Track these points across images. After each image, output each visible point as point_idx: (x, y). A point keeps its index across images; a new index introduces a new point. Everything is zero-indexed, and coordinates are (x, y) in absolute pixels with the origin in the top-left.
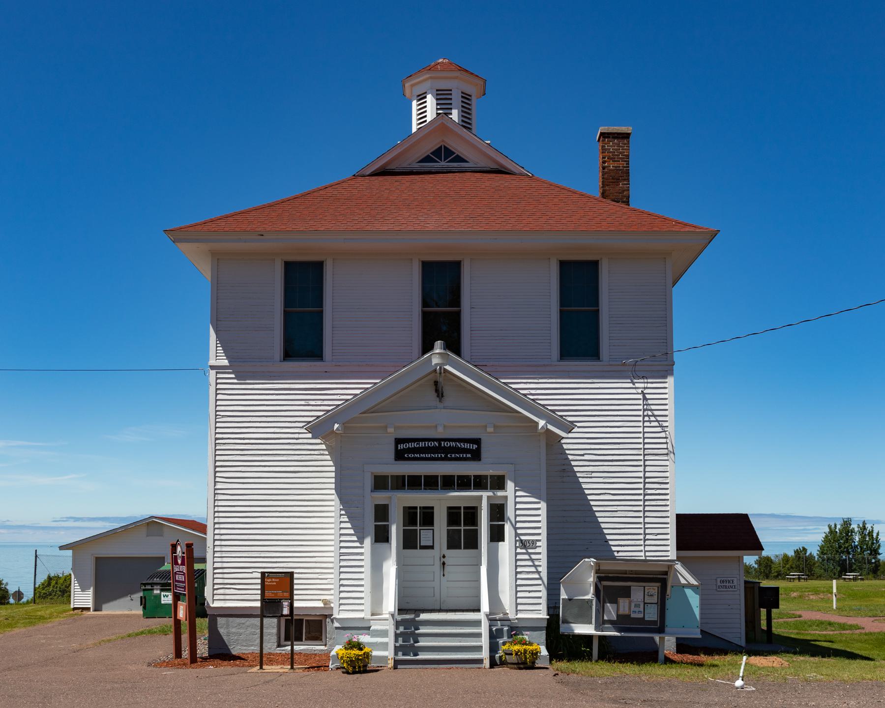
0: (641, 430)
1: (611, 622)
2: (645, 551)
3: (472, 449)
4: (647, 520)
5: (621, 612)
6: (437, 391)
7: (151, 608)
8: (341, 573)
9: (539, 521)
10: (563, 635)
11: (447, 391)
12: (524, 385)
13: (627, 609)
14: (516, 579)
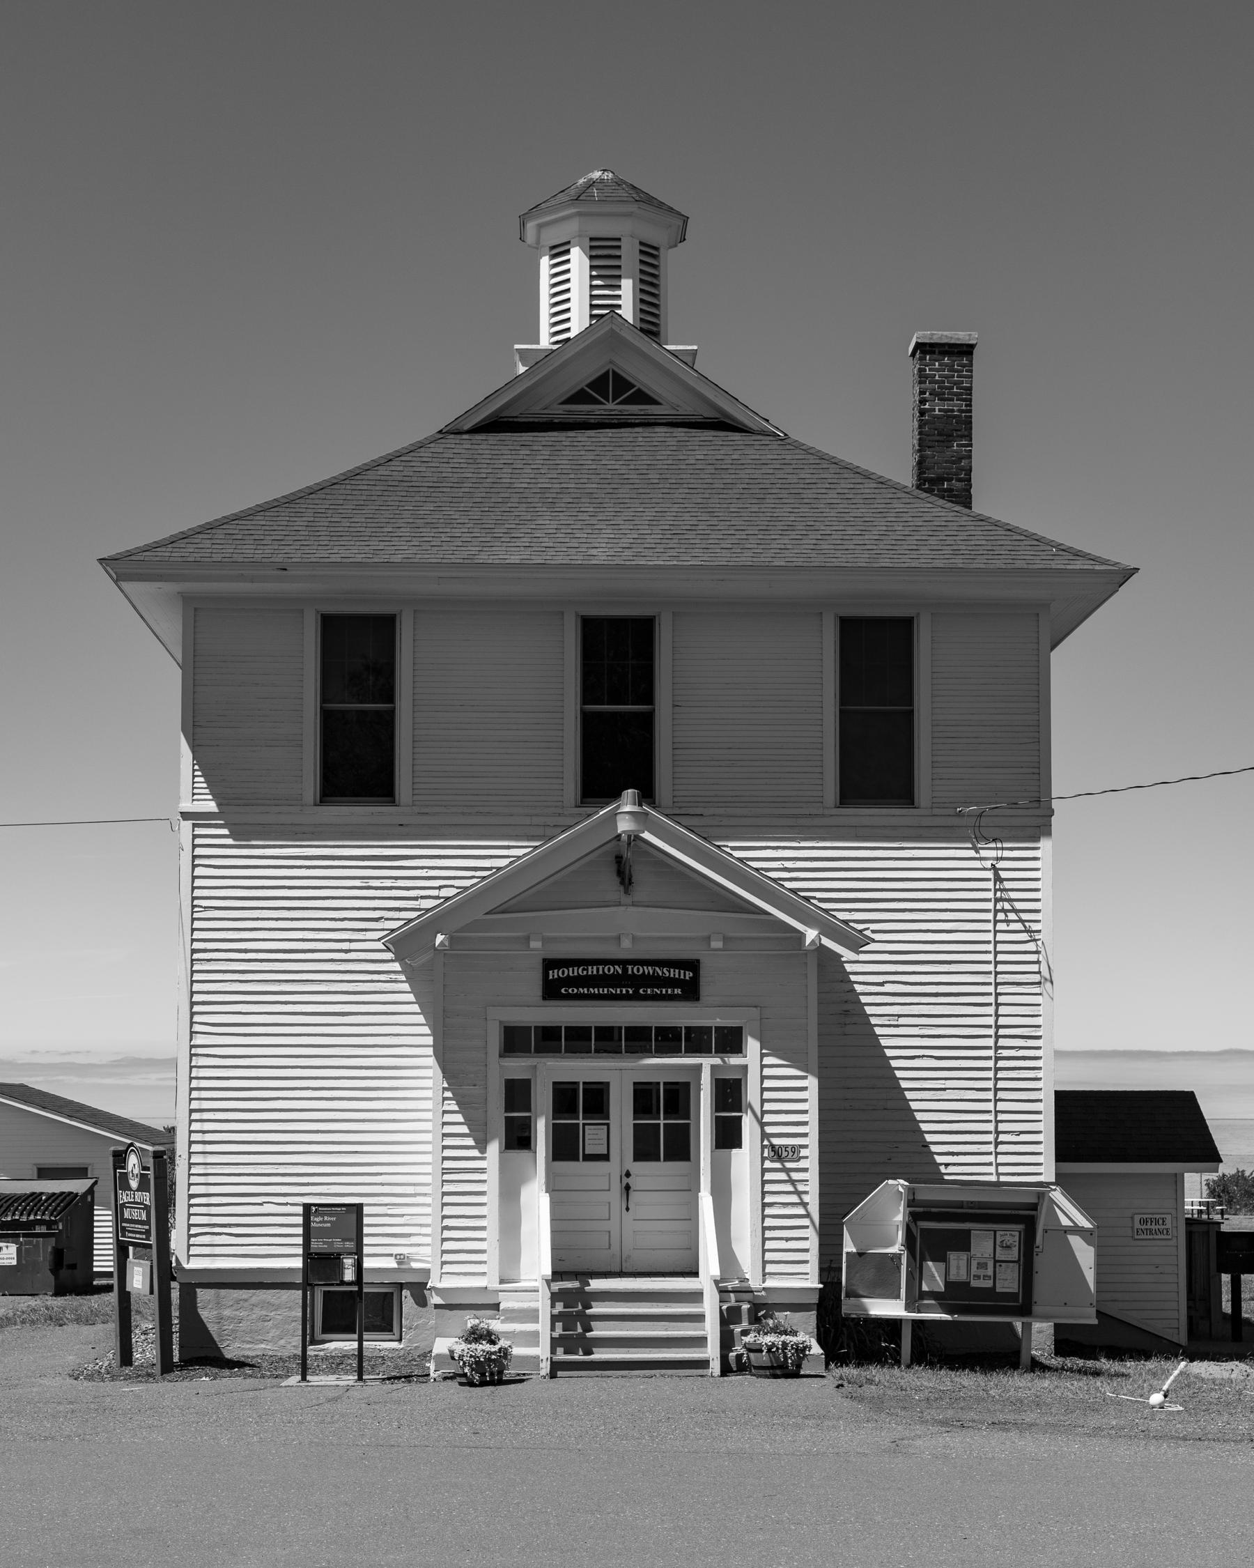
0: (990, 937)
2: (998, 1165)
3: (684, 979)
4: (1001, 1106)
8: (444, 1205)
9: (806, 1112)
10: (848, 1318)
11: (640, 873)
13: (963, 1272)
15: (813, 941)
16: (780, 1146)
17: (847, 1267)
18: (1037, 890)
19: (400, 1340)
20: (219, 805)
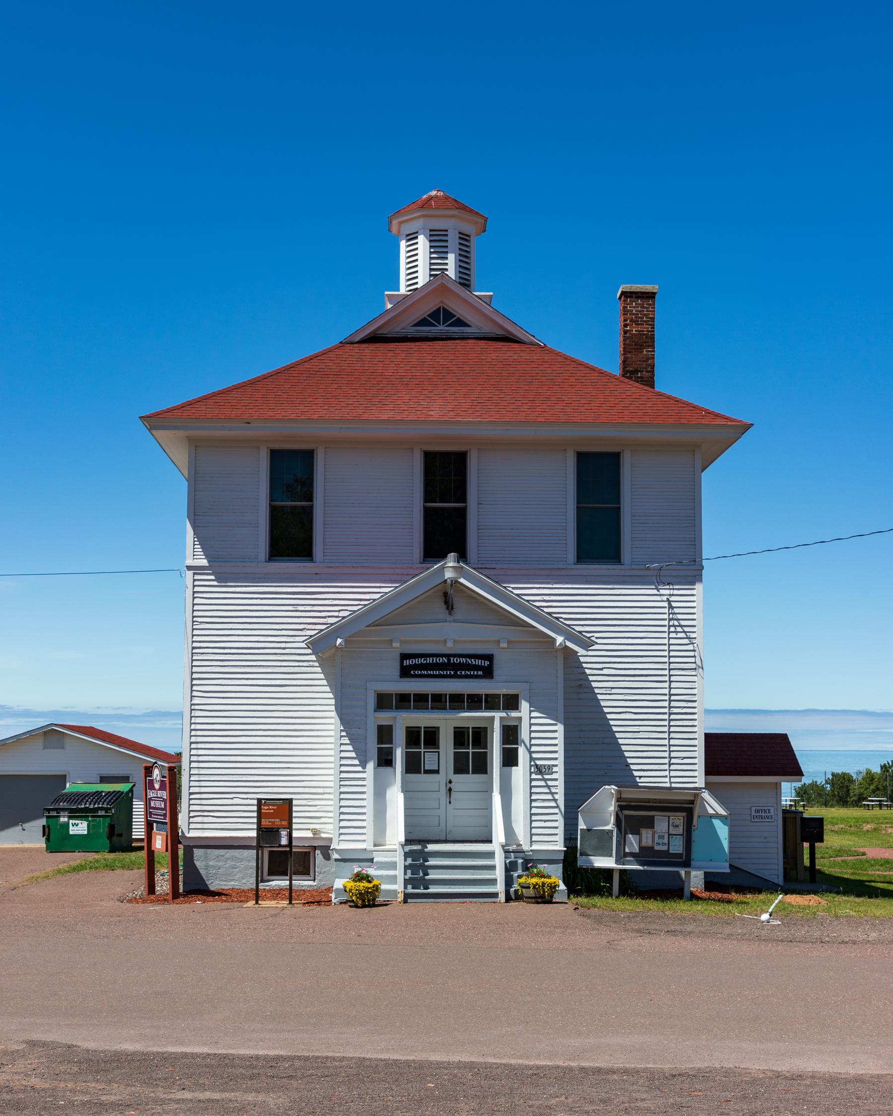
1: (632, 854)
2: (671, 777)
3: (484, 666)
5: (644, 844)
6: (446, 603)
7: (57, 840)
8: (341, 799)
10: (581, 868)
11: (458, 602)
12: (534, 593)
14: (531, 808)
15: (561, 644)
19: (314, 880)
20: (209, 562)
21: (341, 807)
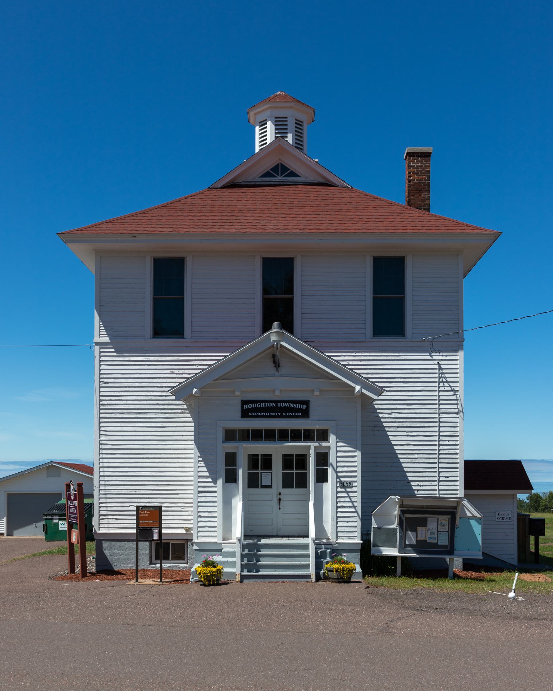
2: (439, 490)
3: (302, 409)
4: (441, 465)
6: (274, 362)
7: (51, 534)
8: (198, 506)
9: (355, 466)
11: (283, 362)
12: (344, 358)
13: (424, 536)
14: (337, 512)
15: (358, 391)
16: (344, 481)
17: (373, 534)
18: (457, 373)
19: (187, 563)
20: (110, 339)
21: (199, 512)
